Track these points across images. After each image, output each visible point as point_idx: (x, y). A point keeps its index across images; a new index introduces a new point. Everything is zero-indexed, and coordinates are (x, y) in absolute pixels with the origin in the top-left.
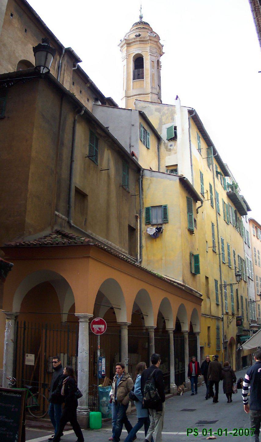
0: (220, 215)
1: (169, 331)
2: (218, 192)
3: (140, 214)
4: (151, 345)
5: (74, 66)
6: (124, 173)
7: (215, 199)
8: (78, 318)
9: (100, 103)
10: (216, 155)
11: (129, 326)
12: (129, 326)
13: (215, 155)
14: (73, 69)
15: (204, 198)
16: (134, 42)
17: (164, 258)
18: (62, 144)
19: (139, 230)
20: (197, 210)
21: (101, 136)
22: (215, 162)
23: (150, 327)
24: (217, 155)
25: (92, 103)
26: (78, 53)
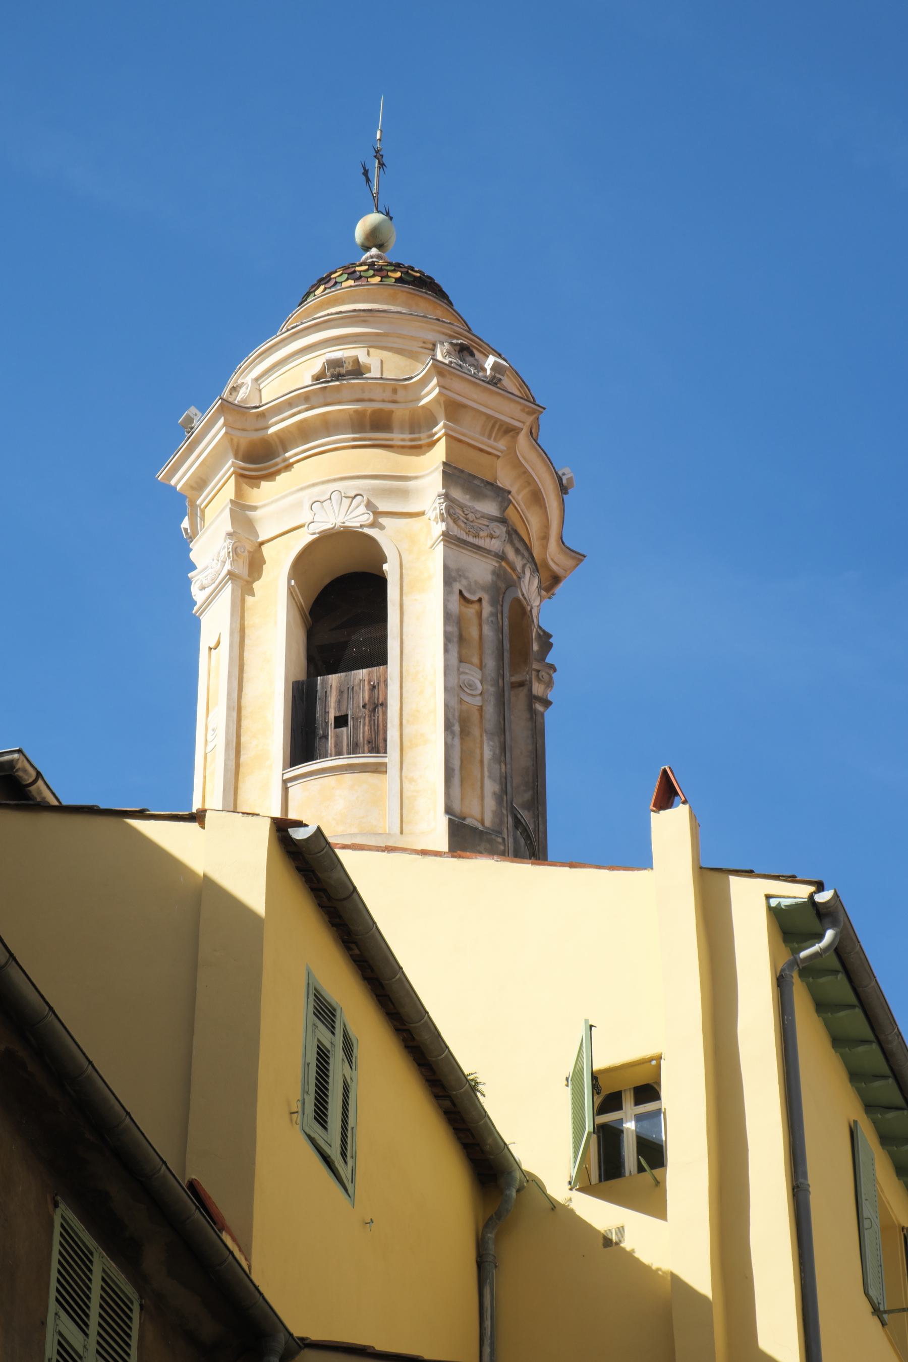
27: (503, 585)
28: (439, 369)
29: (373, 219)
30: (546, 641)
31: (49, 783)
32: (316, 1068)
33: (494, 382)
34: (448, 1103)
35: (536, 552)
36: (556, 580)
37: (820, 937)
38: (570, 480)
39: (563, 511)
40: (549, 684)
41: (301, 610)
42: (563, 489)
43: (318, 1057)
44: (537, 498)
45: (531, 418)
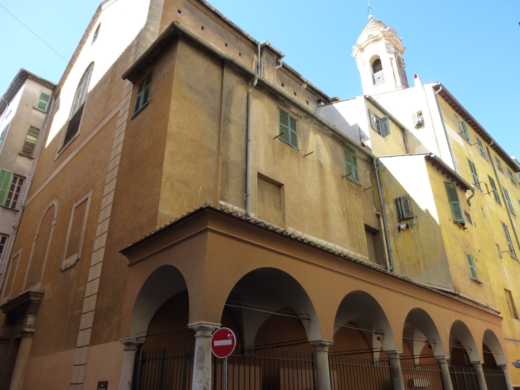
0: (516, 216)
2: (506, 188)
3: (382, 211)
5: (278, 64)
6: (349, 163)
7: (503, 195)
8: (193, 332)
9: (323, 104)
10: (492, 143)
14: (277, 67)
15: (482, 191)
16: (367, 45)
17: (421, 261)
18: (228, 120)
19: (383, 232)
20: (468, 201)
21: (300, 117)
22: (493, 153)
24: (494, 143)
25: (314, 106)
26: (276, 46)
28: (382, 32)
29: (371, 16)
30: (403, 60)
31: (77, 44)
33: (389, 30)
36: (403, 52)
37: (439, 88)
39: (401, 43)
41: (371, 66)
42: (401, 40)
43: (490, 353)
44: (398, 43)
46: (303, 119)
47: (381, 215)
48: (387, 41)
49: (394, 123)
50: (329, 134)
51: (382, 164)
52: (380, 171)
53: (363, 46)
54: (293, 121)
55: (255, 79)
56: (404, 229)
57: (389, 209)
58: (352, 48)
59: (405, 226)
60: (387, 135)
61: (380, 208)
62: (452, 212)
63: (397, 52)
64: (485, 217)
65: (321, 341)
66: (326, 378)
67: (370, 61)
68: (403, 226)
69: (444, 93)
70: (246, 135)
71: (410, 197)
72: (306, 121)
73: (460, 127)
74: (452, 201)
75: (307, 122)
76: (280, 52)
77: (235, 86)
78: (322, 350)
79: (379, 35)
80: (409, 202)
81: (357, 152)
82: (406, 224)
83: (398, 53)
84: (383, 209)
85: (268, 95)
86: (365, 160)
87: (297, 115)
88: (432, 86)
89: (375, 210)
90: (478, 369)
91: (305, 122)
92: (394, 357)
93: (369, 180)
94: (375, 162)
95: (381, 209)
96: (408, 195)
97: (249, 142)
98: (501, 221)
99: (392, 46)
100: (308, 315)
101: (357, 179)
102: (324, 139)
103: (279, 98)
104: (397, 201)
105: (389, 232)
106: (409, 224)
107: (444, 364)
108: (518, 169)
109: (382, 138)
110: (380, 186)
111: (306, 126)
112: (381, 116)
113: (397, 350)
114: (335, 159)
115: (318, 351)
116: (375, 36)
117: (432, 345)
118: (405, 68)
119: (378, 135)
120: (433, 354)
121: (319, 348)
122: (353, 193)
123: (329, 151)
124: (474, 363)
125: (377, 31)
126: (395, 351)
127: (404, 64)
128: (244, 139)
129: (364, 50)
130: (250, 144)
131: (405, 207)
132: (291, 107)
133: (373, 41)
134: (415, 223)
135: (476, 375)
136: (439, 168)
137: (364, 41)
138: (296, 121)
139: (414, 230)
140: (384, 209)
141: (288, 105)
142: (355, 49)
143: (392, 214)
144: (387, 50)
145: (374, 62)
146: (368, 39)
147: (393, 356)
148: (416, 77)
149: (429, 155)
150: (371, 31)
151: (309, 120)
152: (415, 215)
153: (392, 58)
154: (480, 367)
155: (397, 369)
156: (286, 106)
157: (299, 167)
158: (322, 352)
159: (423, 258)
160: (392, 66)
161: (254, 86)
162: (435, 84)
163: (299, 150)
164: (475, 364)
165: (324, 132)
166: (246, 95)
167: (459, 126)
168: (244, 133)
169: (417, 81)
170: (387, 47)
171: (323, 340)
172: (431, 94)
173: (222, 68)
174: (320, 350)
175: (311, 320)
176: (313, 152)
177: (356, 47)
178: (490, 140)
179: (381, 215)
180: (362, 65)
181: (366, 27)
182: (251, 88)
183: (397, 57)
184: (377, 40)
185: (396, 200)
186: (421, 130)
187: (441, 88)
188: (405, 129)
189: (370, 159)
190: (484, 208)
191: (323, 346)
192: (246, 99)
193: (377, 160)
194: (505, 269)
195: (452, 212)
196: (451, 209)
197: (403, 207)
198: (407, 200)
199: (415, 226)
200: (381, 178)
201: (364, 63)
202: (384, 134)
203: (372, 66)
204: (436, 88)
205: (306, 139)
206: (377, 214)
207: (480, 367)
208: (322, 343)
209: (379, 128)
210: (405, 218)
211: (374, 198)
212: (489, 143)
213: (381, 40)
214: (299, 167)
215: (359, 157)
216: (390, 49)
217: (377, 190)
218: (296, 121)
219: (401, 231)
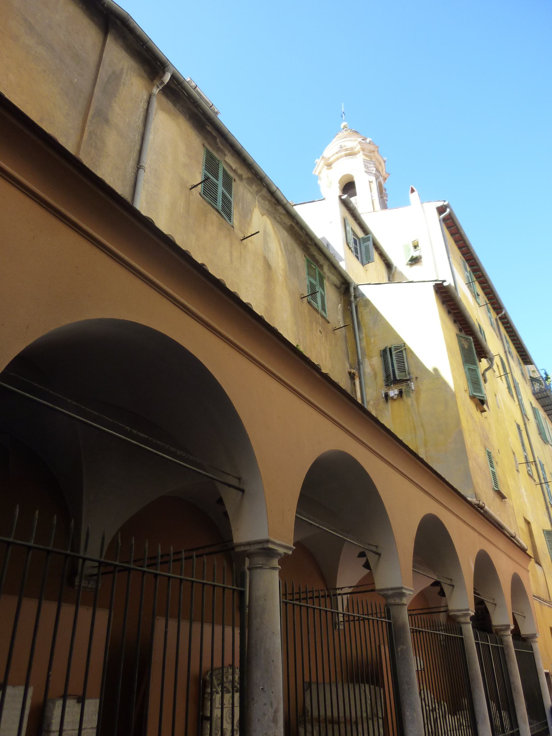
0: (529, 420)
1: (459, 616)
3: (359, 370)
4: (402, 650)
11: (284, 560)
12: (284, 560)
13: (500, 315)
16: (338, 159)
20: (484, 375)
23: (392, 589)
27: (405, 607)
28: (360, 143)
29: (344, 124)
30: (385, 190)
32: (353, 236)
33: (369, 143)
34: (379, 252)
35: (382, 173)
38: (386, 160)
40: (387, 197)
41: (341, 190)
42: (385, 162)
44: (380, 163)
45: (377, 149)
46: (245, 182)
47: (357, 374)
48: (367, 157)
49: (378, 253)
50: (284, 223)
51: (363, 295)
52: (359, 306)
53: (331, 160)
54: (228, 183)
55: (167, 71)
56: (395, 397)
57: (371, 365)
58: (315, 162)
59: (396, 392)
60: (369, 263)
61: (357, 363)
62: (468, 380)
63: (378, 175)
64: (499, 408)
65: (268, 541)
66: (273, 633)
67: (340, 182)
68: (393, 392)
69: (451, 220)
70: (137, 159)
71: (406, 347)
72: (249, 188)
73: (468, 277)
74: (468, 364)
75: (252, 190)
76: (213, 104)
77: (127, 73)
78: (266, 565)
79: (355, 148)
80: (405, 355)
81: (326, 269)
82: (399, 390)
83: (379, 178)
84: (361, 366)
85: (187, 116)
86: (335, 286)
87: (235, 171)
88: (436, 206)
89: (348, 366)
90: (505, 638)
91: (248, 189)
92: (398, 601)
93: (340, 317)
94: (352, 290)
95: (358, 364)
96: (404, 344)
97: (141, 171)
98: (515, 421)
99: (372, 166)
100: (239, 479)
101: (324, 309)
102: (276, 228)
103: (206, 129)
104: (385, 353)
105: (369, 402)
106: (403, 390)
107: (467, 625)
108: (528, 360)
109: (361, 265)
110: (358, 329)
111: (249, 197)
112: (361, 234)
113: (405, 587)
114: (291, 264)
115: (256, 568)
116: (350, 148)
117: (447, 589)
118: (387, 201)
119: (356, 259)
120: (447, 606)
121: (259, 560)
122: (317, 330)
123: (283, 249)
124: (500, 628)
125: (353, 143)
126: (402, 588)
127: (386, 195)
128: (132, 163)
129: (332, 166)
130: (143, 176)
131: (398, 362)
132: (226, 153)
133: (346, 155)
134: (413, 388)
135: (503, 649)
136: (451, 311)
137: (334, 153)
138: (233, 180)
139: (412, 401)
140: (363, 366)
141: (221, 147)
142: (320, 162)
143: (375, 375)
144: (365, 169)
145: (345, 186)
146: (340, 151)
147: (395, 600)
148: (413, 191)
149: (441, 282)
150: (344, 141)
151: (254, 188)
152: (413, 376)
153: (372, 182)
154: (509, 635)
155: (402, 628)
156: (219, 150)
157: (231, 254)
158: (267, 570)
159: (425, 445)
160: (371, 192)
161: (163, 83)
162: (440, 204)
163: (233, 227)
164: (501, 630)
165: (278, 218)
166: (145, 97)
167: (467, 275)
168: (135, 155)
169: (414, 197)
170: (365, 166)
171: (272, 539)
172: (435, 220)
173: (105, 33)
174: (262, 564)
175: (245, 491)
176: (258, 232)
177: (321, 160)
178: (500, 309)
179: (357, 374)
180: (328, 186)
181: (337, 136)
182: (158, 87)
183: (378, 183)
184: (351, 154)
185: (384, 351)
186: (416, 267)
187: (448, 210)
188: (393, 265)
189: (344, 286)
190: (497, 395)
191: (269, 553)
192: (146, 104)
193: (356, 288)
194: (523, 490)
195: (467, 380)
196: (466, 376)
197: (395, 362)
198: (401, 351)
199: (414, 392)
200: (360, 316)
201: (331, 184)
202: (365, 261)
203: (342, 190)
204: (441, 210)
205: (246, 216)
206: (350, 373)
207: (509, 635)
208: (270, 546)
209: (356, 249)
210: (398, 379)
211: (347, 348)
212: (498, 314)
213: (358, 155)
214: (231, 254)
215: (328, 278)
216: (370, 169)
217: (353, 335)
218: (233, 180)
219: (390, 401)
